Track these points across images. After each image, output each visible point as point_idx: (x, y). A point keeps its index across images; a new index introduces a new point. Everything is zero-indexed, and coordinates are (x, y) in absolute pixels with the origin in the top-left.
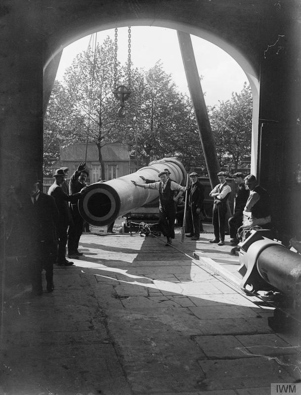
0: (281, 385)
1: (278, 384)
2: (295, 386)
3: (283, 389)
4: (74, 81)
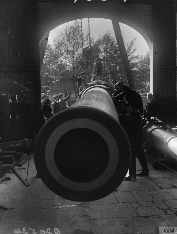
0: (165, 228)
1: (164, 228)
2: (173, 229)
3: (167, 230)
4: (59, 46)
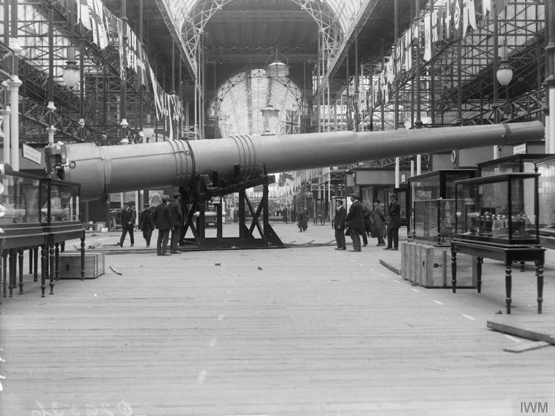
3: (530, 407)
